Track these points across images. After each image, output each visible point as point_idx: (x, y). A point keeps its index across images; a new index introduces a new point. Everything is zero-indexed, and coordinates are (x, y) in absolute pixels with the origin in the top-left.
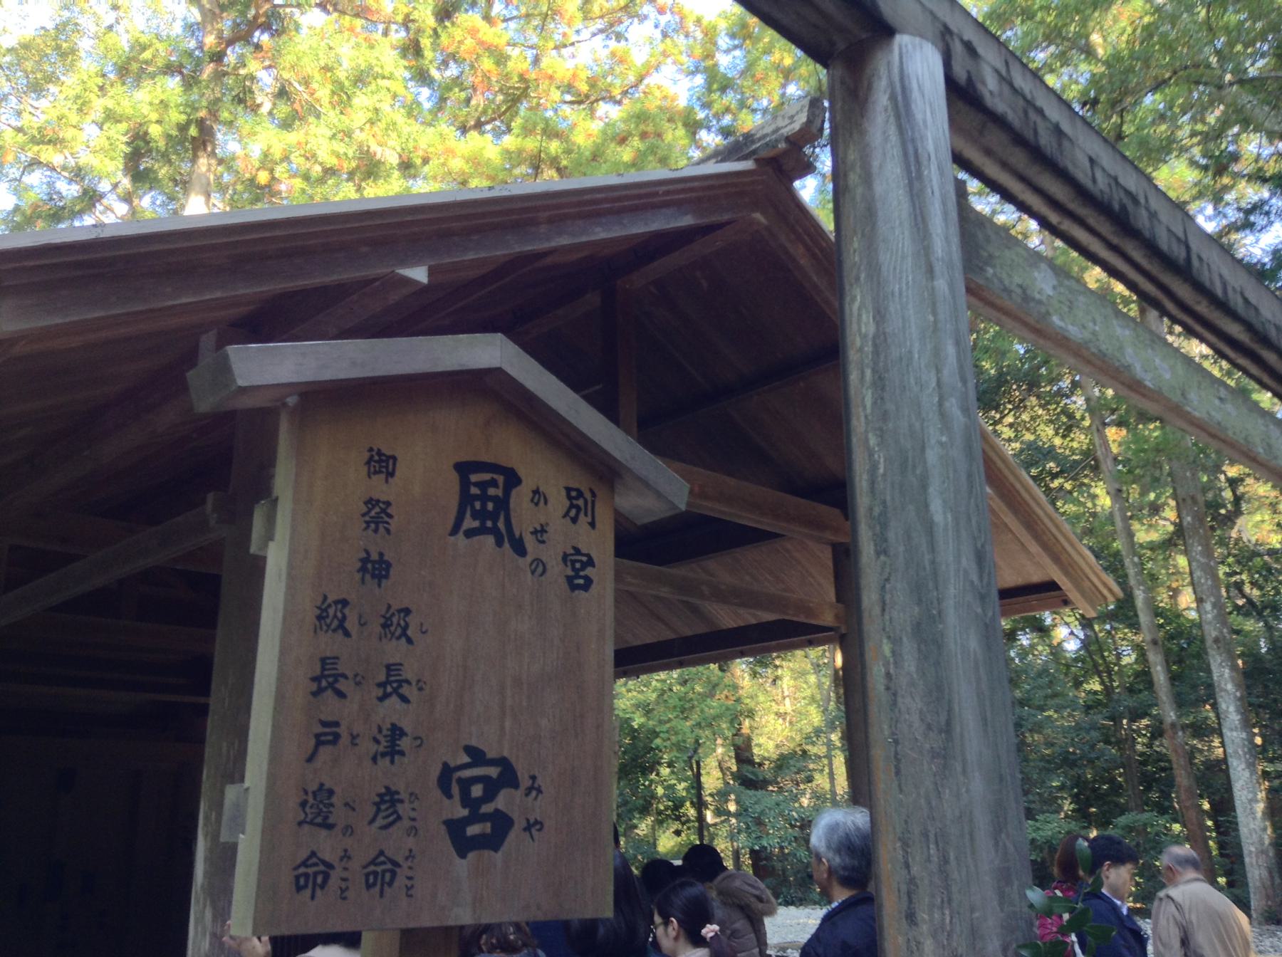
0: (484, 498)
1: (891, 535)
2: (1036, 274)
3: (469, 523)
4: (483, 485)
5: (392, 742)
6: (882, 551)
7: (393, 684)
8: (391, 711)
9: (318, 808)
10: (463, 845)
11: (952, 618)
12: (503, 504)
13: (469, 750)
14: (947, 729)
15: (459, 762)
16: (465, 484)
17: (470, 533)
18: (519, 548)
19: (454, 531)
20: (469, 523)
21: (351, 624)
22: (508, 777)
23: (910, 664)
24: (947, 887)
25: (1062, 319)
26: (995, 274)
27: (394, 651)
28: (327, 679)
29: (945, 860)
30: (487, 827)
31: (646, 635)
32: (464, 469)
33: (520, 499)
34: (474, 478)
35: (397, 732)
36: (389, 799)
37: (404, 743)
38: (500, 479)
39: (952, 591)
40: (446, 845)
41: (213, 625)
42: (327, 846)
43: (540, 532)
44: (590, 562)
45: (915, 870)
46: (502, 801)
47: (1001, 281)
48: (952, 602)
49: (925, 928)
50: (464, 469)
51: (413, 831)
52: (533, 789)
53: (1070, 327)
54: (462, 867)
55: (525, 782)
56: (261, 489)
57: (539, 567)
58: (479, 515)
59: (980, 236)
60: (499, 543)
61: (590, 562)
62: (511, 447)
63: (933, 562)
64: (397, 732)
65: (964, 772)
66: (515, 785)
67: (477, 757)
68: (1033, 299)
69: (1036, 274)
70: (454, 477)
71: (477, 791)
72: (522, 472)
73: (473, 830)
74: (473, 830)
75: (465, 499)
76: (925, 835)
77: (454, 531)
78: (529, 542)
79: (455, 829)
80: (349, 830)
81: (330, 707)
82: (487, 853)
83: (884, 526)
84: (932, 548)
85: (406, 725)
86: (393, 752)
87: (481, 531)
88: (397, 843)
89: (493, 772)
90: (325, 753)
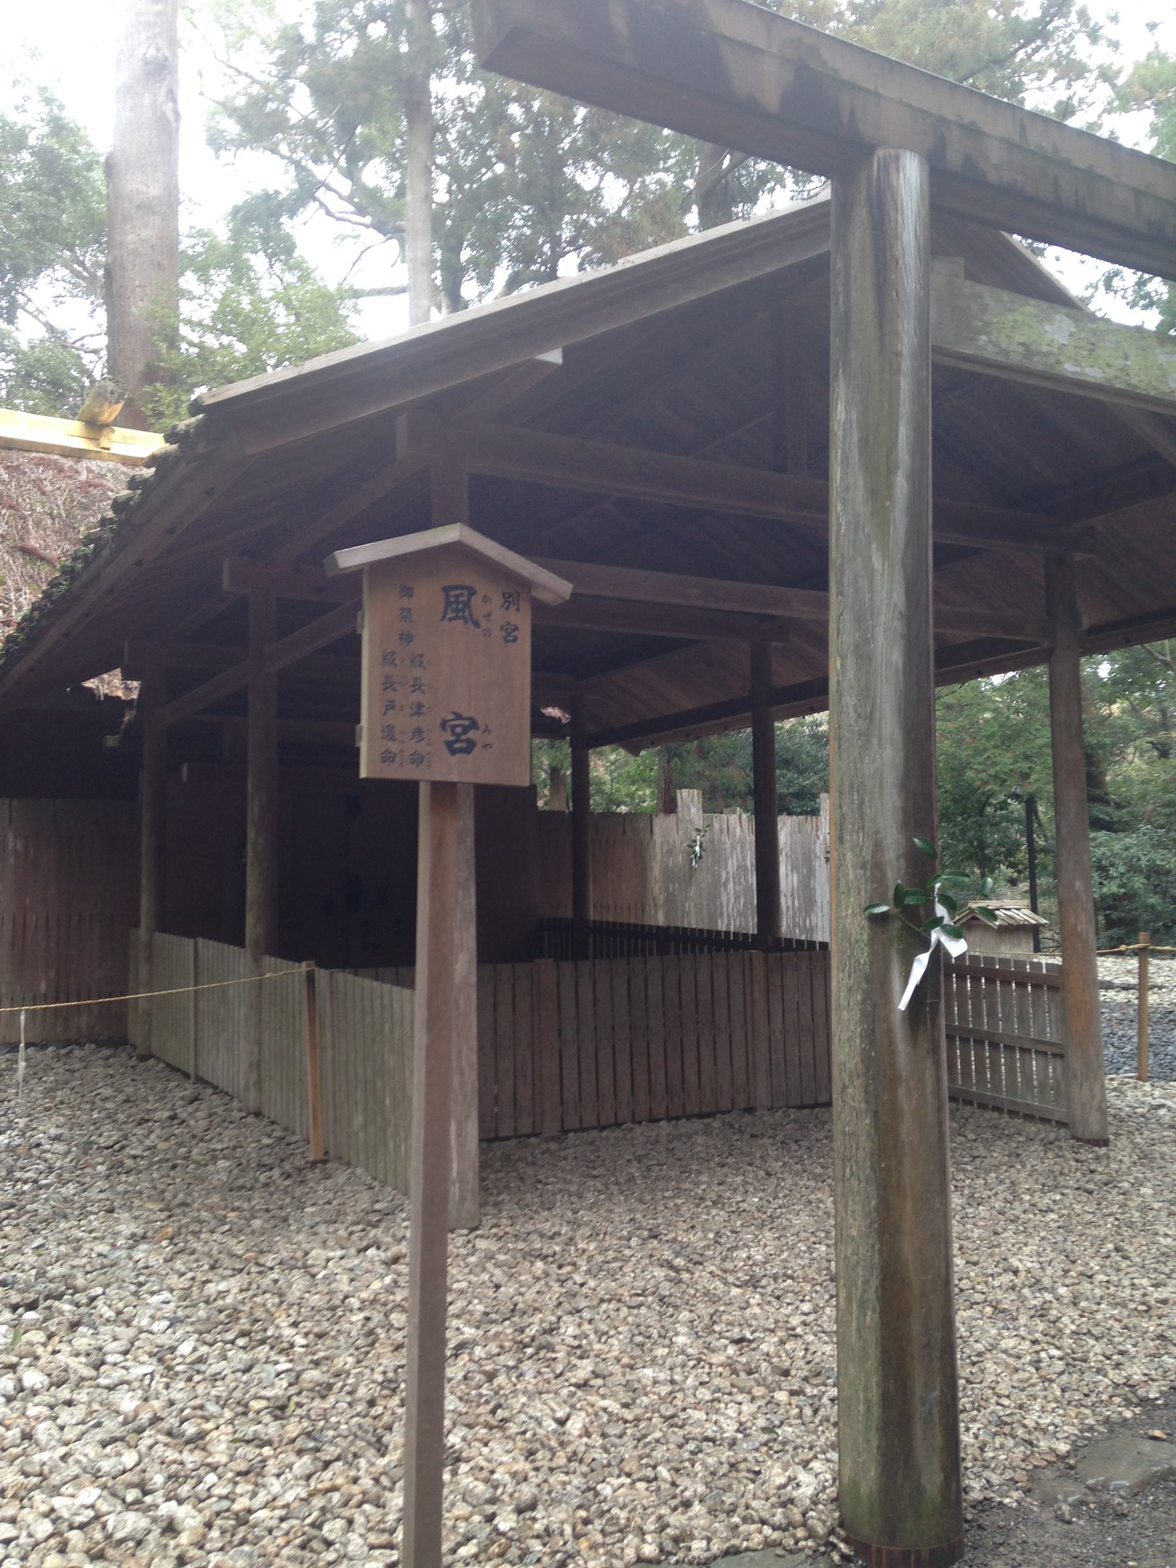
0: (458, 603)
1: (846, 581)
2: (1047, 328)
3: (450, 615)
4: (457, 597)
5: (419, 709)
6: (840, 593)
7: (417, 686)
8: (417, 697)
9: (389, 733)
10: (453, 752)
11: (880, 638)
12: (467, 604)
13: (454, 713)
14: (871, 717)
15: (745, 757)
16: (447, 597)
17: (451, 619)
18: (477, 625)
19: (444, 618)
20: (450, 615)
21: (398, 661)
22: (473, 725)
23: (851, 674)
24: (862, 819)
25: (1077, 363)
26: (990, 341)
27: (417, 672)
28: (388, 684)
29: (862, 803)
30: (464, 745)
31: (961, 636)
32: (447, 590)
33: (476, 601)
34: (453, 593)
35: (420, 706)
36: (418, 731)
37: (424, 710)
38: (466, 592)
39: (883, 618)
40: (445, 751)
41: (825, 587)
42: (394, 747)
43: (488, 616)
44: (516, 629)
45: (845, 809)
46: (471, 735)
47: (996, 345)
48: (881, 628)
49: (848, 845)
50: (447, 590)
51: (430, 744)
52: (487, 730)
53: (1088, 370)
54: (454, 759)
55: (482, 728)
56: (359, 606)
57: (487, 633)
58: (456, 610)
59: (975, 307)
60: (466, 622)
61: (516, 629)
62: (468, 578)
63: (871, 599)
64: (420, 706)
65: (880, 745)
66: (477, 728)
67: (458, 716)
68: (1039, 353)
69: (1047, 328)
70: (442, 595)
71: (459, 730)
72: (477, 588)
73: (457, 745)
74: (457, 745)
75: (448, 604)
76: (851, 786)
77: (444, 618)
78: (482, 621)
79: (449, 745)
80: (402, 742)
81: (391, 695)
82: (464, 756)
83: (842, 574)
84: (872, 589)
85: (425, 702)
86: (419, 713)
87: (457, 618)
88: (422, 747)
89: (467, 723)
90: (390, 712)
